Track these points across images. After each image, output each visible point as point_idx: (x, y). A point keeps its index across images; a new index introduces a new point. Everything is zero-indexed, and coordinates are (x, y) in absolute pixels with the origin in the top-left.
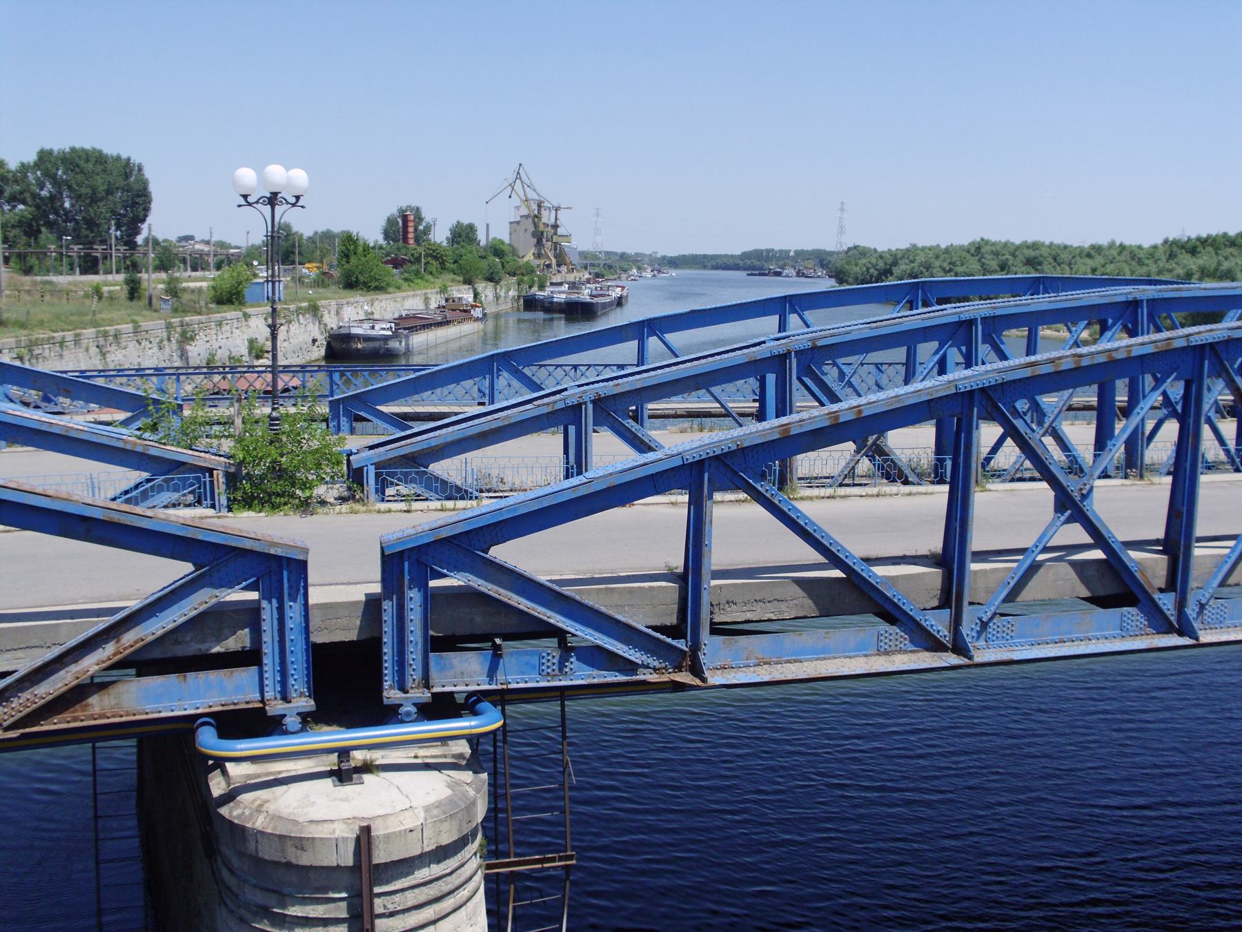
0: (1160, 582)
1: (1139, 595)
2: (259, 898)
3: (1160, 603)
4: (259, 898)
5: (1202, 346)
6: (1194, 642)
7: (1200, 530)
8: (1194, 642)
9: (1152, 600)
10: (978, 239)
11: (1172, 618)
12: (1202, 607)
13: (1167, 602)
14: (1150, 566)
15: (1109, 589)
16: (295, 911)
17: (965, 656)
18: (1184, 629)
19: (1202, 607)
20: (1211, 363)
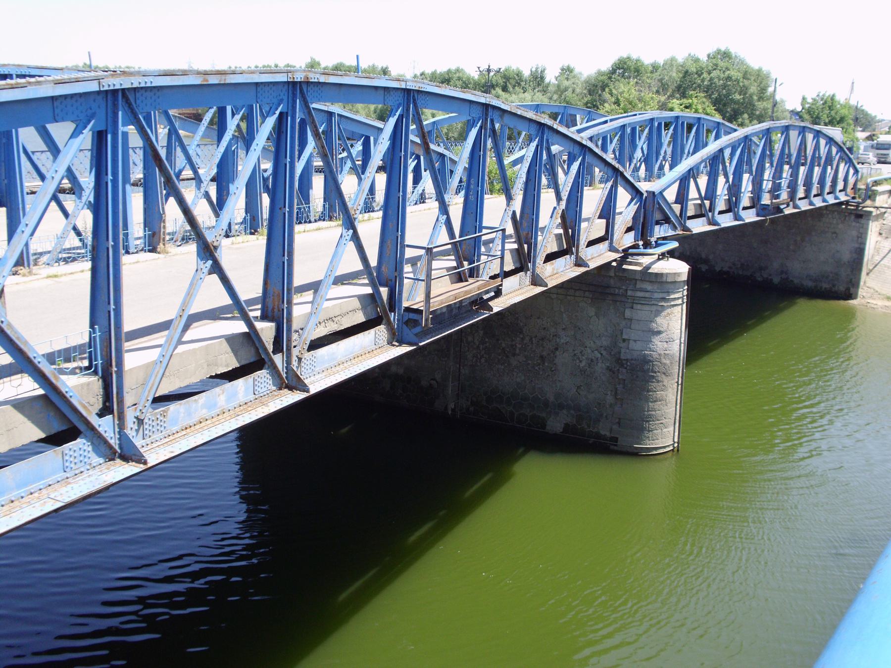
0: (98, 404)
1: (81, 427)
2: (661, 295)
3: (100, 430)
4: (661, 295)
5: (115, 92)
6: (141, 467)
7: (129, 324)
8: (141, 467)
9: (92, 429)
10: (625, 56)
11: (112, 442)
12: (300, 359)
13: (106, 426)
14: (80, 388)
15: (57, 427)
16: (672, 297)
17: (304, 391)
18: (128, 454)
19: (300, 359)
20: (124, 112)
